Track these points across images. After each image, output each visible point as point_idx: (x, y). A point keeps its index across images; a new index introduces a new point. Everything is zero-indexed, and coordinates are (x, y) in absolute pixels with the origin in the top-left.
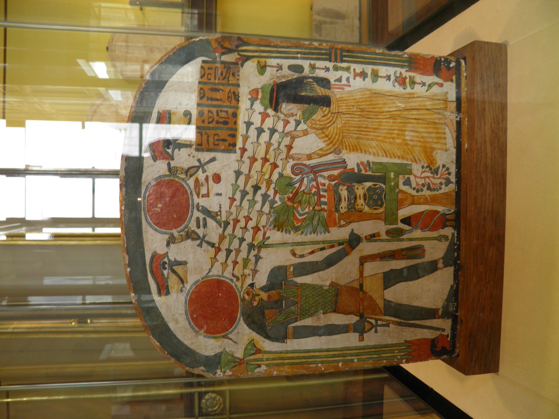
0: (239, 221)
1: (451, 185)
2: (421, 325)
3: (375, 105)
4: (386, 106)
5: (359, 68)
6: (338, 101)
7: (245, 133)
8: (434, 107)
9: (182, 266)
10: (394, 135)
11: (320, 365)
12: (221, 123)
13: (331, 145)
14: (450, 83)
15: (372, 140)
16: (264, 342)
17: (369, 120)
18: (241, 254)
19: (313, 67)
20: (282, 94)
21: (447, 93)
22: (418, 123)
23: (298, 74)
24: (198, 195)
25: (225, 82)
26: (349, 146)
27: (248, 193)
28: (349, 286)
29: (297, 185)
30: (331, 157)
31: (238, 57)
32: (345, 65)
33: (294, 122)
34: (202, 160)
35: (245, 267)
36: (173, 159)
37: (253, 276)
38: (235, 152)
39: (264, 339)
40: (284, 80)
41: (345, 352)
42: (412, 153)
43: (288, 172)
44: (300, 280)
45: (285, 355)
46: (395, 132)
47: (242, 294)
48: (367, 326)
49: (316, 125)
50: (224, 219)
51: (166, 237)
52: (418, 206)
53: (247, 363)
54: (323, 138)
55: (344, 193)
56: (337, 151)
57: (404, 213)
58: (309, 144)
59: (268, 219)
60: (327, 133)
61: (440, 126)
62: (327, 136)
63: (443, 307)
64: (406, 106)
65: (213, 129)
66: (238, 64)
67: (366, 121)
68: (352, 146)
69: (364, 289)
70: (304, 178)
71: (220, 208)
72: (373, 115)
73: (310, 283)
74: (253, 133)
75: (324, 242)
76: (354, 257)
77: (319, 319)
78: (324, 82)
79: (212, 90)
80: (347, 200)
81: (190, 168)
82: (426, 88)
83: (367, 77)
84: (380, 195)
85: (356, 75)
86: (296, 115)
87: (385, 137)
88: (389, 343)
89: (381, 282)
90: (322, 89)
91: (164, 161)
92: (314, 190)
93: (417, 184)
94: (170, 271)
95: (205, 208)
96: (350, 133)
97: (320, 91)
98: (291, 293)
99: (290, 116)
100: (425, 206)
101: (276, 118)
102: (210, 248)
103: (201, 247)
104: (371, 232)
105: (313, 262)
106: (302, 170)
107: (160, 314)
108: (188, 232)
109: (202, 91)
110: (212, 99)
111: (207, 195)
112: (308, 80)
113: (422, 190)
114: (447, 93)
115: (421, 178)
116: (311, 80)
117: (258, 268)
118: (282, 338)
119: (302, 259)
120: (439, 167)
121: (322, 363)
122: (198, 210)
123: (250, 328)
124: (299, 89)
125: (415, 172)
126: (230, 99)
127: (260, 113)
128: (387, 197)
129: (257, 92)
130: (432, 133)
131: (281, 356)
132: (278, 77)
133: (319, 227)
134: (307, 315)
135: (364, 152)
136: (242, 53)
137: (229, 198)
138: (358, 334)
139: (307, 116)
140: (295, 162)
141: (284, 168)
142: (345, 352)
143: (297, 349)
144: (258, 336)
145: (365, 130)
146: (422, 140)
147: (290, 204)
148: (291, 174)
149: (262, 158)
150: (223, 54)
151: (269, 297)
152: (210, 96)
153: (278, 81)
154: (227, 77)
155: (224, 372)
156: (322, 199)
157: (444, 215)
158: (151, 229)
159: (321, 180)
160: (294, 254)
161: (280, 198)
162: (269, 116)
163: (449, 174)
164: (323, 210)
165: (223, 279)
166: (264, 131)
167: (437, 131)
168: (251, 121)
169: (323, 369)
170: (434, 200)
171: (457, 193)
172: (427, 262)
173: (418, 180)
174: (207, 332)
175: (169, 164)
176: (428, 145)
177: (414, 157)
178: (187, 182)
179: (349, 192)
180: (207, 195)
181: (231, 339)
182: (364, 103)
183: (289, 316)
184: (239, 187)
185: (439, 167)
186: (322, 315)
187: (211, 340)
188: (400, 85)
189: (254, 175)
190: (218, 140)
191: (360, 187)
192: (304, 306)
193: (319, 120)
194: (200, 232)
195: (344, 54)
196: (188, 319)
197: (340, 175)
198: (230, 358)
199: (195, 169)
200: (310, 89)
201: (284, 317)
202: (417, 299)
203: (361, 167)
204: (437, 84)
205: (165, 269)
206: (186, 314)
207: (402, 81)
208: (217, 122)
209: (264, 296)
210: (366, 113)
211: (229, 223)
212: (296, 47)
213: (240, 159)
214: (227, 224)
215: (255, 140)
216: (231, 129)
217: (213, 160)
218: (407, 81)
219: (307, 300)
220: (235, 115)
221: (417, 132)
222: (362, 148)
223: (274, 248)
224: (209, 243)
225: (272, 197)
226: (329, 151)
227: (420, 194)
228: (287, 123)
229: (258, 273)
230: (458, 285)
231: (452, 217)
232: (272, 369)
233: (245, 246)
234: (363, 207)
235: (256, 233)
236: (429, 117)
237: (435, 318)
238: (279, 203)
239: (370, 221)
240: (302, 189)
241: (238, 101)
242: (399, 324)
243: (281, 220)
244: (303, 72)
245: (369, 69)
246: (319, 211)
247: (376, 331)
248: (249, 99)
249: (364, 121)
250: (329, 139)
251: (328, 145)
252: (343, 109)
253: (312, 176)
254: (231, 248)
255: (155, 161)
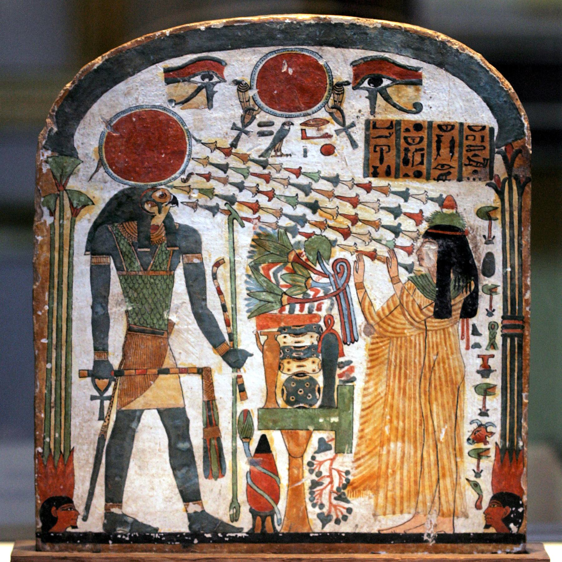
0: (268, 182)
1: (320, 524)
2: (97, 476)
3: (441, 390)
4: (440, 408)
5: (496, 363)
6: (444, 329)
7: (393, 189)
8: (442, 492)
9: (206, 101)
10: (395, 422)
11: (47, 307)
12: (406, 155)
13: (377, 319)
14: (483, 523)
15: (388, 386)
16: (89, 220)
17: (418, 381)
18: (221, 185)
19: (492, 291)
20: (451, 244)
21: (467, 517)
22: (416, 463)
23: (481, 267)
24: (305, 124)
25: (465, 161)
26: (377, 348)
27: (307, 195)
28: (166, 351)
29: (318, 268)
30: (360, 320)
31: (502, 179)
32: (499, 340)
33: (411, 263)
34: (353, 129)
35: (203, 191)
36: (354, 88)
37: (187, 204)
38: (365, 177)
39: (93, 220)
40: (471, 246)
41: (64, 348)
42: (369, 453)
43: (338, 253)
44: (179, 273)
45: (66, 253)
46: (401, 424)
47: (163, 187)
48: (102, 383)
49: (407, 296)
50: (271, 160)
51: (248, 80)
52: (288, 467)
53: (59, 195)
54: (388, 306)
55: (307, 340)
56: (369, 330)
57: (276, 439)
58: (378, 285)
59: (270, 225)
60: (395, 312)
61: (413, 503)
62: (391, 313)
63: (124, 515)
64: (441, 443)
65: (398, 145)
66: (491, 179)
67: (415, 376)
68: (378, 353)
69: (161, 376)
70: (329, 277)
71: (287, 155)
72: (425, 387)
73: (174, 289)
74: (393, 201)
75: (234, 309)
76: (209, 357)
77: (118, 304)
78: (469, 310)
79: (452, 142)
80: (297, 345)
81: (342, 112)
82: (472, 478)
83: (483, 376)
84: (303, 399)
85: (485, 359)
86: (421, 265)
87: (392, 406)
88: (73, 422)
89: (171, 404)
90: (460, 305)
91: (352, 77)
92: (311, 293)
93: (321, 463)
94: (199, 85)
95: (287, 134)
96: (396, 349)
97: (457, 302)
98: (161, 260)
99: (418, 256)
100: (287, 478)
101: (414, 235)
102: (230, 141)
103: (232, 129)
104: (247, 385)
105: (205, 294)
106: (340, 275)
107: (139, 71)
108: (254, 110)
109: (449, 128)
110: (439, 142)
111: (304, 137)
112: (472, 282)
113: (311, 471)
114: (467, 517)
115: (331, 470)
116: (473, 287)
117: (199, 210)
118: (93, 248)
119: (211, 277)
120: (348, 502)
121: (50, 312)
122: (284, 124)
123: (112, 200)
124: (459, 270)
125: (340, 458)
126: (439, 167)
127: (421, 211)
128: (301, 411)
129: (452, 208)
130: (402, 489)
131: (64, 246)
132: (475, 237)
133: (257, 302)
134: (125, 285)
135: (369, 371)
136: (507, 183)
137: (300, 168)
138: (91, 367)
139: (418, 281)
140: (352, 264)
141: (344, 248)
142: (64, 348)
143: (75, 272)
144: (99, 212)
145: (402, 375)
146: (390, 471)
147: (292, 256)
148: (335, 258)
149: (356, 214)
150: (505, 158)
151: (157, 227)
152: (443, 139)
153: (469, 238)
154: (471, 163)
155: (47, 162)
156: (298, 307)
157: (272, 514)
158: (258, 59)
159: (326, 303)
160: (218, 264)
161: (299, 242)
162: (417, 225)
163: (337, 522)
164: (282, 307)
165: (186, 159)
166: (395, 218)
167: (405, 499)
168: (410, 198)
169: (40, 313)
170: (296, 493)
171: (307, 535)
172: (197, 484)
173: (327, 464)
174: (109, 137)
175: (348, 83)
176: (382, 482)
177: (363, 457)
178: (323, 109)
179: (309, 348)
180: (304, 137)
181: (96, 171)
182: (442, 371)
183: (126, 258)
184: (316, 181)
185: (348, 502)
186: (124, 309)
187: (97, 143)
188: (474, 432)
189: (332, 203)
190: (382, 150)
191: (315, 367)
192: (140, 281)
193: (414, 300)
194: (253, 127)
195: (516, 339)
196: (130, 109)
197: (334, 333)
198: (68, 170)
199: (341, 120)
200: (459, 286)
201: (124, 250)
202: (140, 467)
203: (346, 368)
204: (480, 498)
205: (203, 78)
206: (137, 107)
207: (480, 435)
208: (407, 150)
209: (159, 220)
210: (428, 375)
211: (264, 168)
212: (521, 265)
213: (355, 182)
214: (264, 165)
215: (383, 205)
216: (397, 169)
217: (354, 144)
218: (482, 446)
219: (148, 286)
220: (418, 175)
221: (402, 462)
222: (375, 369)
223: (227, 235)
224: (237, 139)
225: (301, 230)
226: (368, 316)
227: (306, 468)
228: (409, 251)
229: (193, 211)
230: (159, 541)
231: (269, 529)
232: (45, 234)
233: (232, 191)
234: (285, 371)
235: (249, 208)
236: (427, 483)
237: (107, 500)
238: (293, 241)
239: (265, 384)
240: (312, 275)
241: (438, 179)
242: (102, 438)
243: (268, 243)
244: (484, 274)
245: (495, 379)
246: (281, 302)
247: (93, 398)
248: (441, 195)
249: (415, 372)
250: (387, 317)
251: (378, 315)
252: (433, 338)
253: (332, 290)
254: (230, 171)
255: (351, 64)
